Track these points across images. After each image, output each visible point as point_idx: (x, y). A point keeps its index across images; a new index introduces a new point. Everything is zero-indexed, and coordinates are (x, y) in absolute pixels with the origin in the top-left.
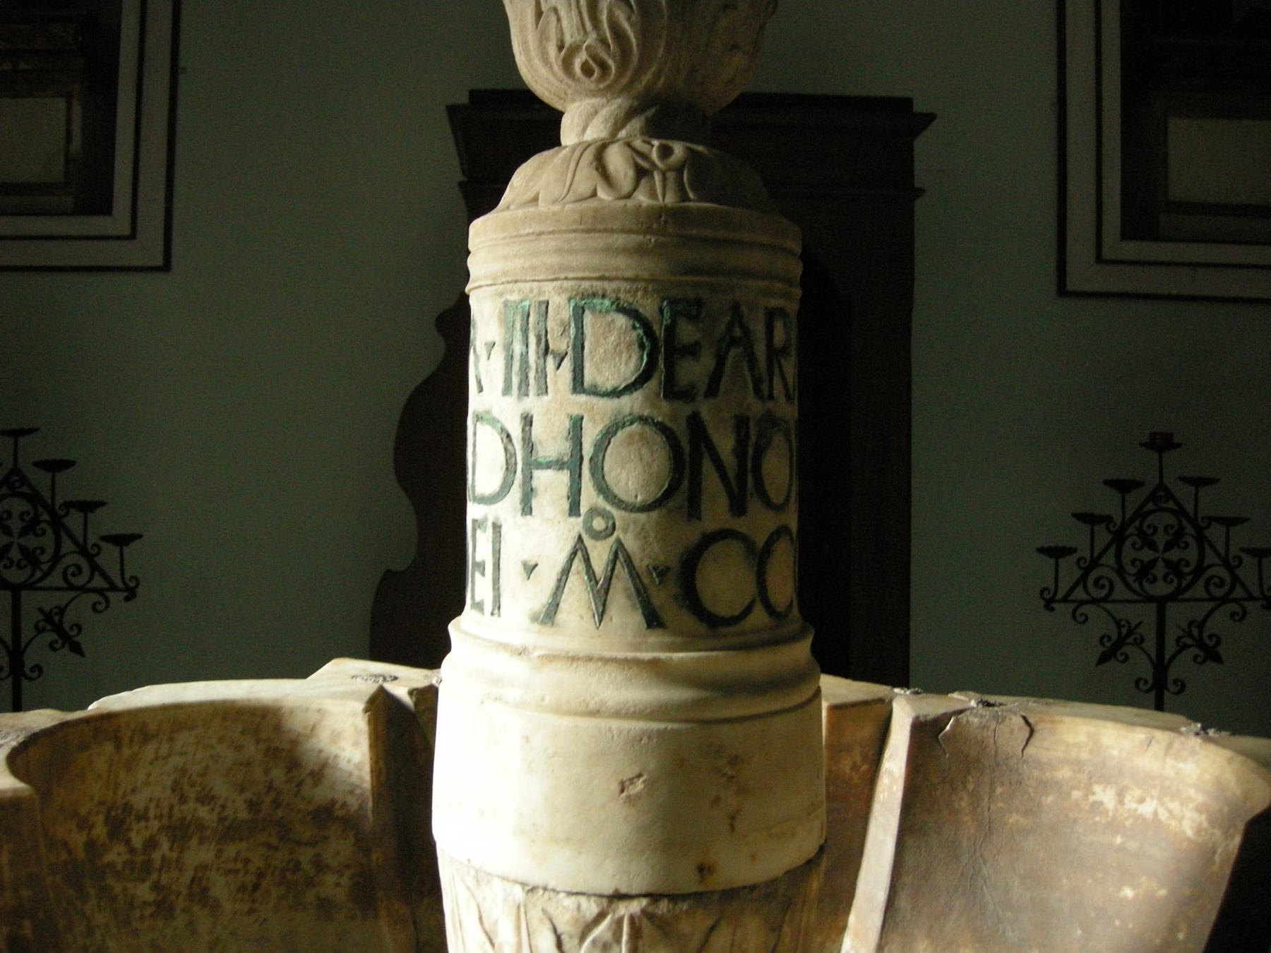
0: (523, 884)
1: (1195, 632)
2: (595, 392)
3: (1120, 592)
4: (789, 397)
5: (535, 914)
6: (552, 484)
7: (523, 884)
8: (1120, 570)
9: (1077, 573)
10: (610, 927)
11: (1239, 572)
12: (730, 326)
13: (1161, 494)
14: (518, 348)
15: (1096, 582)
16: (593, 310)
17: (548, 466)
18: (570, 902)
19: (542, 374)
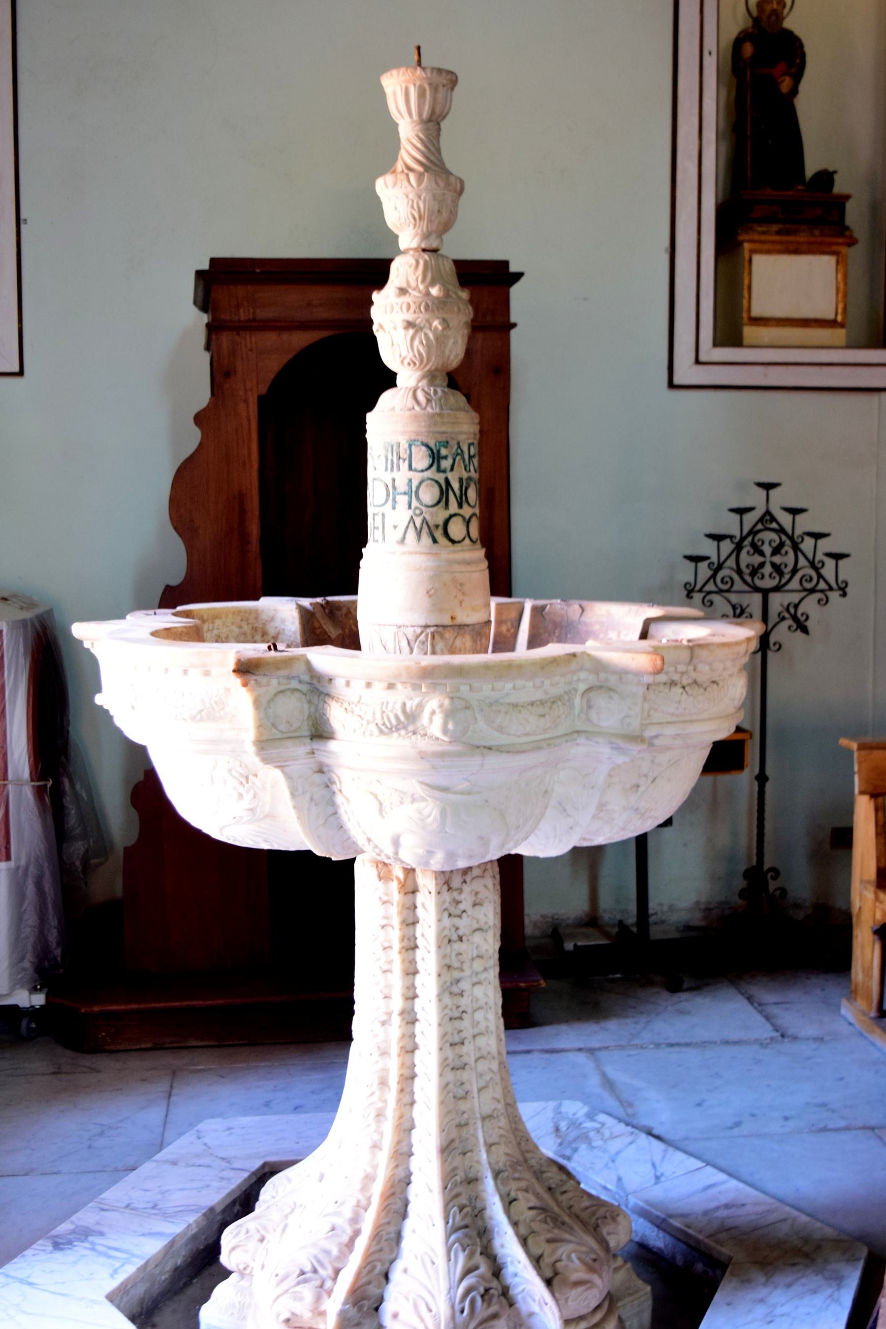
0: (397, 626)
1: (792, 610)
2: (416, 470)
3: (739, 585)
4: (475, 471)
5: (401, 634)
6: (403, 500)
7: (397, 626)
8: (739, 572)
9: (710, 573)
10: (424, 636)
11: (823, 571)
12: (457, 450)
13: (768, 517)
14: (390, 457)
15: (722, 580)
16: (415, 445)
17: (401, 494)
18: (411, 629)
19: (398, 465)
